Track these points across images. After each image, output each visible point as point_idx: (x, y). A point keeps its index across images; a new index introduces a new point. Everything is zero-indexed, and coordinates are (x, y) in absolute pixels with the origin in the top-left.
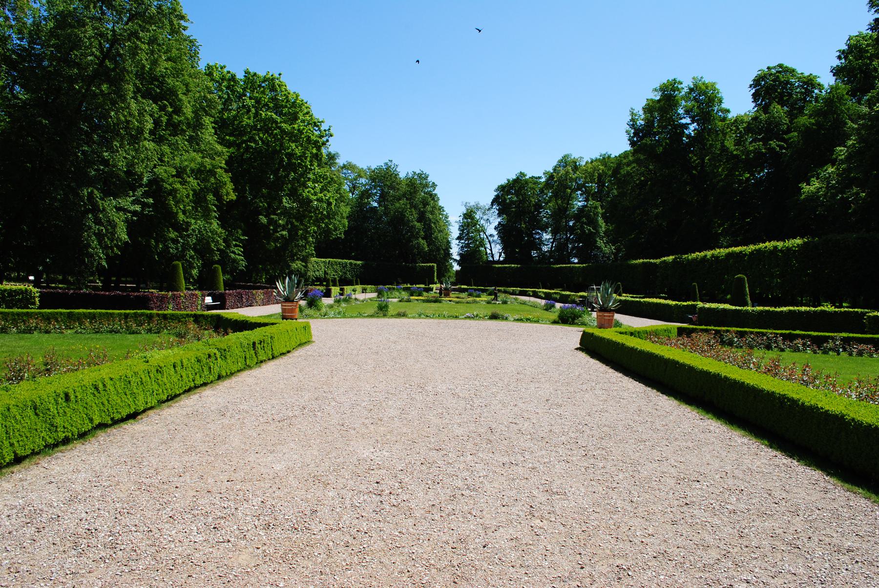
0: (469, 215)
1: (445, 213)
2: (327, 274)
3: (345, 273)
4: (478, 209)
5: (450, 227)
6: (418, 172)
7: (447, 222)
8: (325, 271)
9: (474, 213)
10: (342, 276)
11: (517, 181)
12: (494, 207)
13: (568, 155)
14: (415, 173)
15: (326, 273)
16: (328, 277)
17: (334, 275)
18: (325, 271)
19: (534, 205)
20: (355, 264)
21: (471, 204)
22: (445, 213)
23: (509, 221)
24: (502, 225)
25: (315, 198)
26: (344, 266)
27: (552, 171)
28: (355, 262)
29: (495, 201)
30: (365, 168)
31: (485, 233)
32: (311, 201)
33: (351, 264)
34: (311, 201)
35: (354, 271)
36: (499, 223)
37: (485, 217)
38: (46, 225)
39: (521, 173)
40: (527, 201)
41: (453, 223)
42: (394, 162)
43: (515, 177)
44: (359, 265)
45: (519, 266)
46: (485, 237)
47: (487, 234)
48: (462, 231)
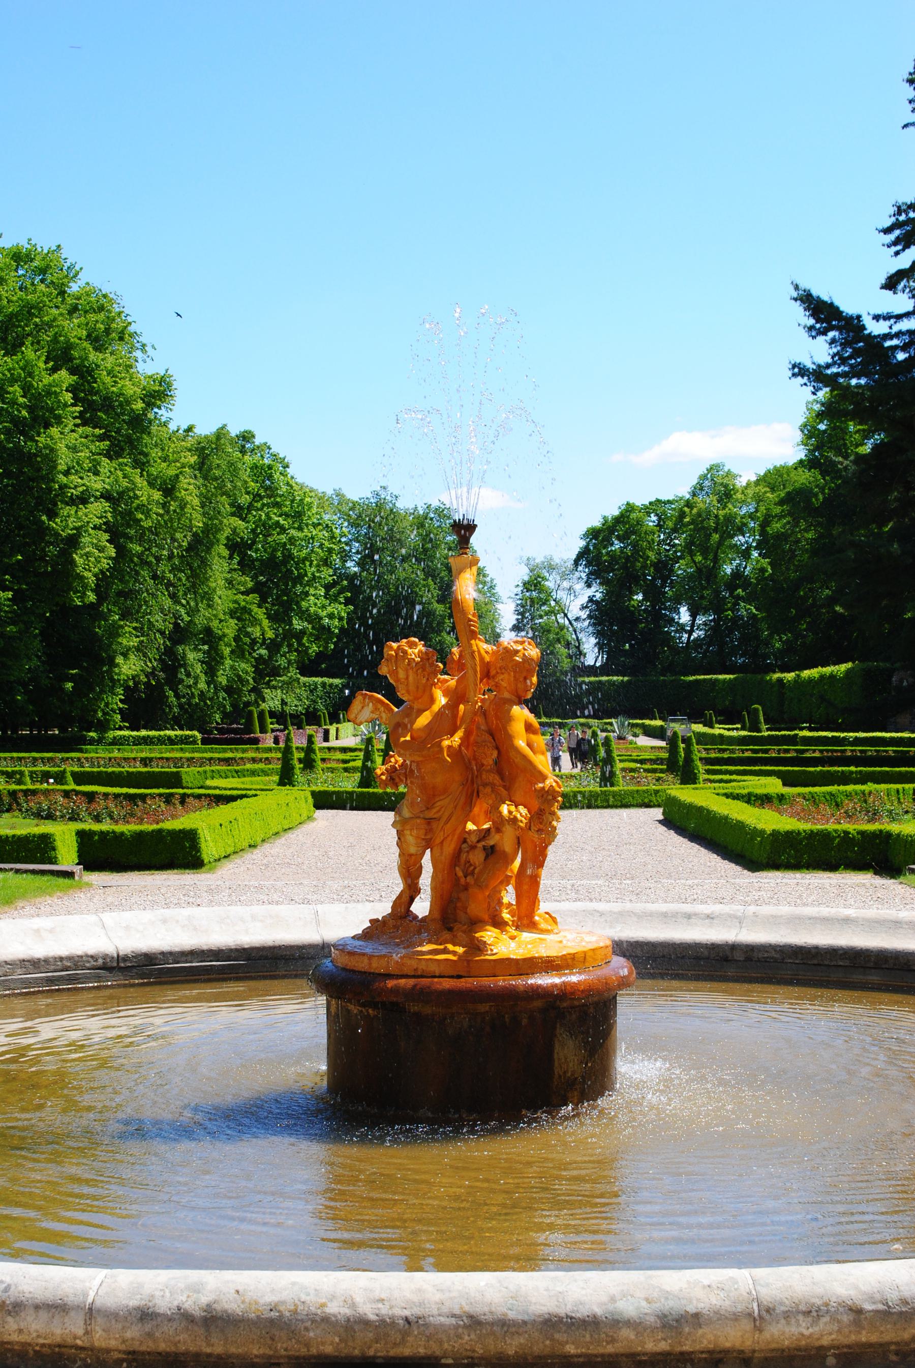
0: (534, 584)
1: (488, 579)
2: (286, 704)
3: (315, 702)
4: (551, 568)
5: (499, 606)
6: (435, 504)
7: (493, 594)
8: (283, 700)
9: (544, 579)
10: (309, 707)
11: (621, 519)
12: (580, 568)
13: (718, 466)
14: (429, 507)
15: (283, 703)
16: (287, 709)
17: (296, 706)
18: (283, 700)
19: (655, 565)
20: (331, 685)
21: (537, 561)
22: (488, 579)
23: (608, 594)
24: (597, 603)
25: (324, 613)
26: (312, 690)
27: (688, 496)
28: (331, 680)
29: (583, 554)
30: (330, 492)
31: (566, 615)
32: (321, 618)
33: (324, 685)
34: (321, 618)
35: (329, 697)
36: (591, 600)
37: (566, 584)
38: (69, 685)
39: (628, 504)
40: (641, 557)
41: (504, 598)
42: (391, 489)
43: (616, 513)
44: (337, 686)
45: (626, 679)
46: (567, 622)
47: (570, 616)
48: (522, 614)
